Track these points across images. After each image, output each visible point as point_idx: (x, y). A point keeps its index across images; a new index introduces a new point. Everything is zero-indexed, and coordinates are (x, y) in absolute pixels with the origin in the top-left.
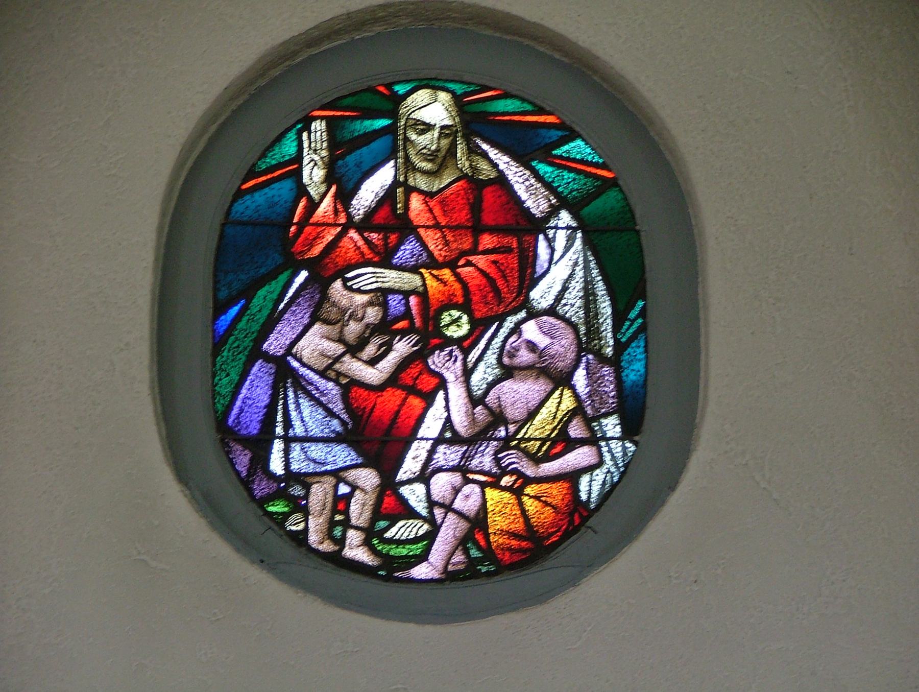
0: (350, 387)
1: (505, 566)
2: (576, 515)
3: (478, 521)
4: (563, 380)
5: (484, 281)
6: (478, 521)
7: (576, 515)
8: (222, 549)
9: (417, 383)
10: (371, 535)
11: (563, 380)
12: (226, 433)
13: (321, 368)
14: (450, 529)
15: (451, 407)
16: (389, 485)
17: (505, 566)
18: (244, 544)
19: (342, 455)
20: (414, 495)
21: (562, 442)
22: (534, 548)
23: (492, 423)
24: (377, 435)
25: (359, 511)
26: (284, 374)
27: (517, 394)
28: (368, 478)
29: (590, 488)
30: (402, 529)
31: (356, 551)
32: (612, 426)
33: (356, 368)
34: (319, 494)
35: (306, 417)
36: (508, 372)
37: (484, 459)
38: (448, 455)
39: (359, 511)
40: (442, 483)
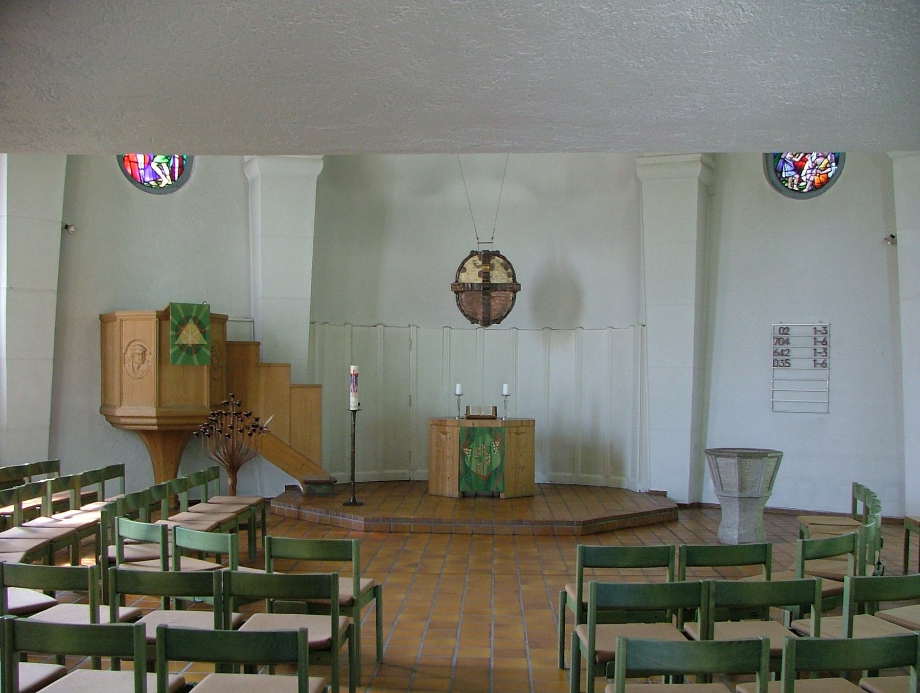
0: (794, 162)
1: (817, 188)
2: (828, 179)
3: (813, 181)
4: (826, 158)
5: (267, 529)
6: (813, 181)
7: (828, 179)
8: (774, 191)
9: (804, 160)
10: (798, 185)
11: (826, 158)
12: (776, 171)
13: (273, 554)
14: (809, 183)
15: (809, 164)
16: (800, 177)
17: (817, 188)
18: (773, 184)
19: (793, 173)
20: (804, 178)
21: (826, 168)
22: (822, 185)
23: (815, 165)
24: (798, 169)
25: (796, 182)
26: (785, 161)
27: (819, 160)
28: (797, 176)
29: (830, 175)
30: (803, 184)
31: (796, 188)
32: (834, 164)
33: (795, 159)
34: (790, 179)
35: (788, 167)
36: (818, 157)
37: (814, 171)
38: (809, 171)
39: (796, 182)
40: (808, 176)
